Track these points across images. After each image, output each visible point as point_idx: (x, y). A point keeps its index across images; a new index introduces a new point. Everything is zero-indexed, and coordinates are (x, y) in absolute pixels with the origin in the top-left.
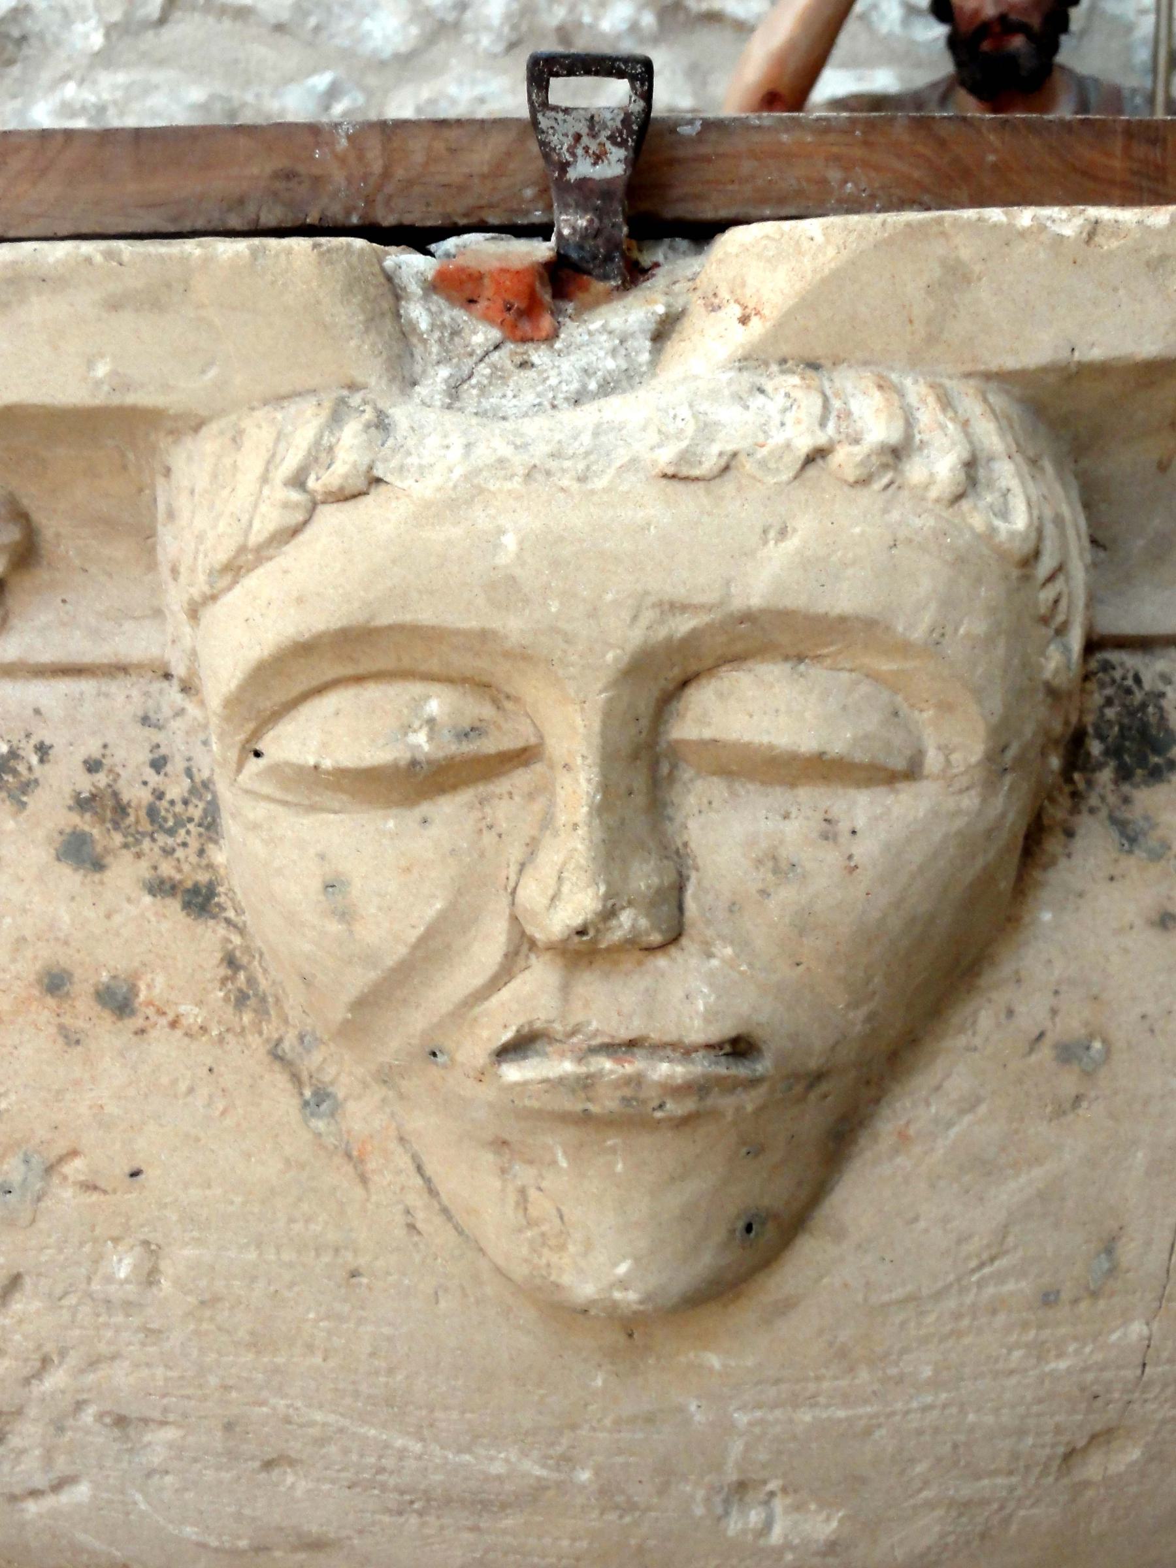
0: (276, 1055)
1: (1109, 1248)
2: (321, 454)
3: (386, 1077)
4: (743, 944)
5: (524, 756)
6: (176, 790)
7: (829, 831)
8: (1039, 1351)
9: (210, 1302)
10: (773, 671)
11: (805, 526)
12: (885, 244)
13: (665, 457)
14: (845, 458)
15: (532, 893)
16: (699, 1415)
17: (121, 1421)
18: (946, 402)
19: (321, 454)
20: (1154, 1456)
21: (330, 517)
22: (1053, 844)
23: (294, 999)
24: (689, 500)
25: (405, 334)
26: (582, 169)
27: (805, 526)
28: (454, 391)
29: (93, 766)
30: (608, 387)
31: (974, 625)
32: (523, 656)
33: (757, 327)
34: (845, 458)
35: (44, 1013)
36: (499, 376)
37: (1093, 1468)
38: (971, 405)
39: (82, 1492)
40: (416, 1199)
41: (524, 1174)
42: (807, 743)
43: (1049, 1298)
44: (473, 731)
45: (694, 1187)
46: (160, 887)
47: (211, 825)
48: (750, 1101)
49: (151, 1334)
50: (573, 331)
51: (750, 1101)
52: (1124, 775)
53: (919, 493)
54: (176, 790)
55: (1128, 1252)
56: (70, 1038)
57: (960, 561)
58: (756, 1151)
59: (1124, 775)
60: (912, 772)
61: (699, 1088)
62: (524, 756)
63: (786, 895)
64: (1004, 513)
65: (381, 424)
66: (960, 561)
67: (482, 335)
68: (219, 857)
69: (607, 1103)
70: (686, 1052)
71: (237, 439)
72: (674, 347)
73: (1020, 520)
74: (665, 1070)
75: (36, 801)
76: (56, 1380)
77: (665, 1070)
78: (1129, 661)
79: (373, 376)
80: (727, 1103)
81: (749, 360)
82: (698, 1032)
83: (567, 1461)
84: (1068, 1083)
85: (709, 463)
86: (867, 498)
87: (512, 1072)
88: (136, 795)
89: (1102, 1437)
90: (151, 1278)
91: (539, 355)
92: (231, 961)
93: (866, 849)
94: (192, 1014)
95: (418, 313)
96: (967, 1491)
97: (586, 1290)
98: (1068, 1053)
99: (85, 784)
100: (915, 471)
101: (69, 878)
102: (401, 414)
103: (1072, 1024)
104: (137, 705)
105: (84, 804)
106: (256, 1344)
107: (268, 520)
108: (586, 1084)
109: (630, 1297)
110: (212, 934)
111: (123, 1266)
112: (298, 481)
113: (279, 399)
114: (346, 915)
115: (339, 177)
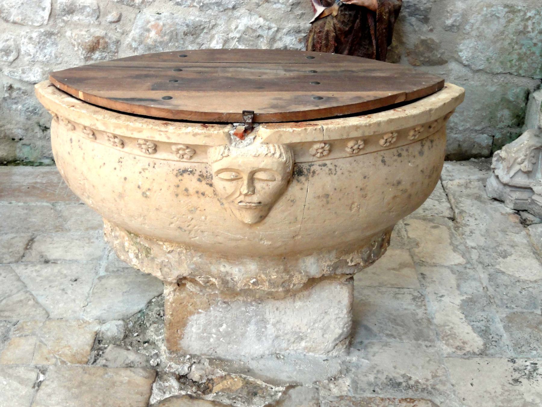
0: (218, 200)
1: (296, 218)
2: (224, 152)
3: (229, 203)
4: (260, 194)
5: (241, 178)
6: (209, 175)
7: (267, 185)
8: (290, 227)
9: (211, 221)
10: (263, 172)
11: (265, 161)
12: (274, 133)
13: (253, 154)
14: (269, 155)
15: (242, 190)
16: (257, 232)
17: (202, 232)
18: (279, 148)
19: (224, 152)
20: (302, 237)
21: (225, 158)
22: (291, 182)
23: (220, 195)
24: (256, 158)
25: (231, 139)
26: (247, 121)
27: (265, 161)
28: (235, 145)
29: (200, 172)
30: (249, 144)
31: (280, 169)
32: (241, 171)
33: (263, 140)
34: (269, 155)
35: (196, 195)
36: (239, 143)
37: (296, 238)
38: (281, 147)
39: (198, 238)
40: (231, 213)
41: (241, 212)
42: (265, 179)
43: (290, 223)
44: (237, 176)
45: (256, 214)
46: (207, 184)
47: (212, 178)
48: (261, 207)
49: (206, 224)
50: (246, 138)
51: (261, 207)
52: (298, 175)
53: (275, 158)
54: (209, 175)
55: (298, 219)
56: (199, 197)
57: (279, 163)
58: (261, 211)
59: (298, 175)
60: (275, 180)
61: (256, 206)
62: (241, 178)
63: (263, 191)
64: (283, 159)
65: (229, 150)
66: (279, 163)
67: (238, 139)
68: (213, 181)
69: (248, 207)
70: (255, 203)
71: (216, 149)
72: (255, 140)
73: (285, 159)
74: (253, 205)
75: (195, 175)
76: (196, 228)
77: (253, 205)
78: (299, 164)
79: (228, 144)
80: (258, 207)
81: (262, 143)
82: (256, 201)
83: (245, 236)
84: (292, 204)
85: (257, 155)
86: (271, 158)
87: (240, 204)
88: (205, 175)
89: (297, 235)
90: (206, 219)
91: (243, 141)
92: (214, 191)
93: (271, 187)
94: (210, 196)
95: (232, 137)
96: (283, 240)
97: (246, 222)
98: (292, 201)
99: (200, 174)
100: (275, 155)
101: (198, 182)
102: (231, 148)
103: (292, 198)
104: (205, 166)
105: (200, 175)
106: (216, 225)
107: (219, 158)
108: (246, 206)
109: (250, 223)
110: (212, 188)
111: (203, 218)
112: (222, 155)
113: (220, 145)
114: (225, 190)
115: (224, 118)
